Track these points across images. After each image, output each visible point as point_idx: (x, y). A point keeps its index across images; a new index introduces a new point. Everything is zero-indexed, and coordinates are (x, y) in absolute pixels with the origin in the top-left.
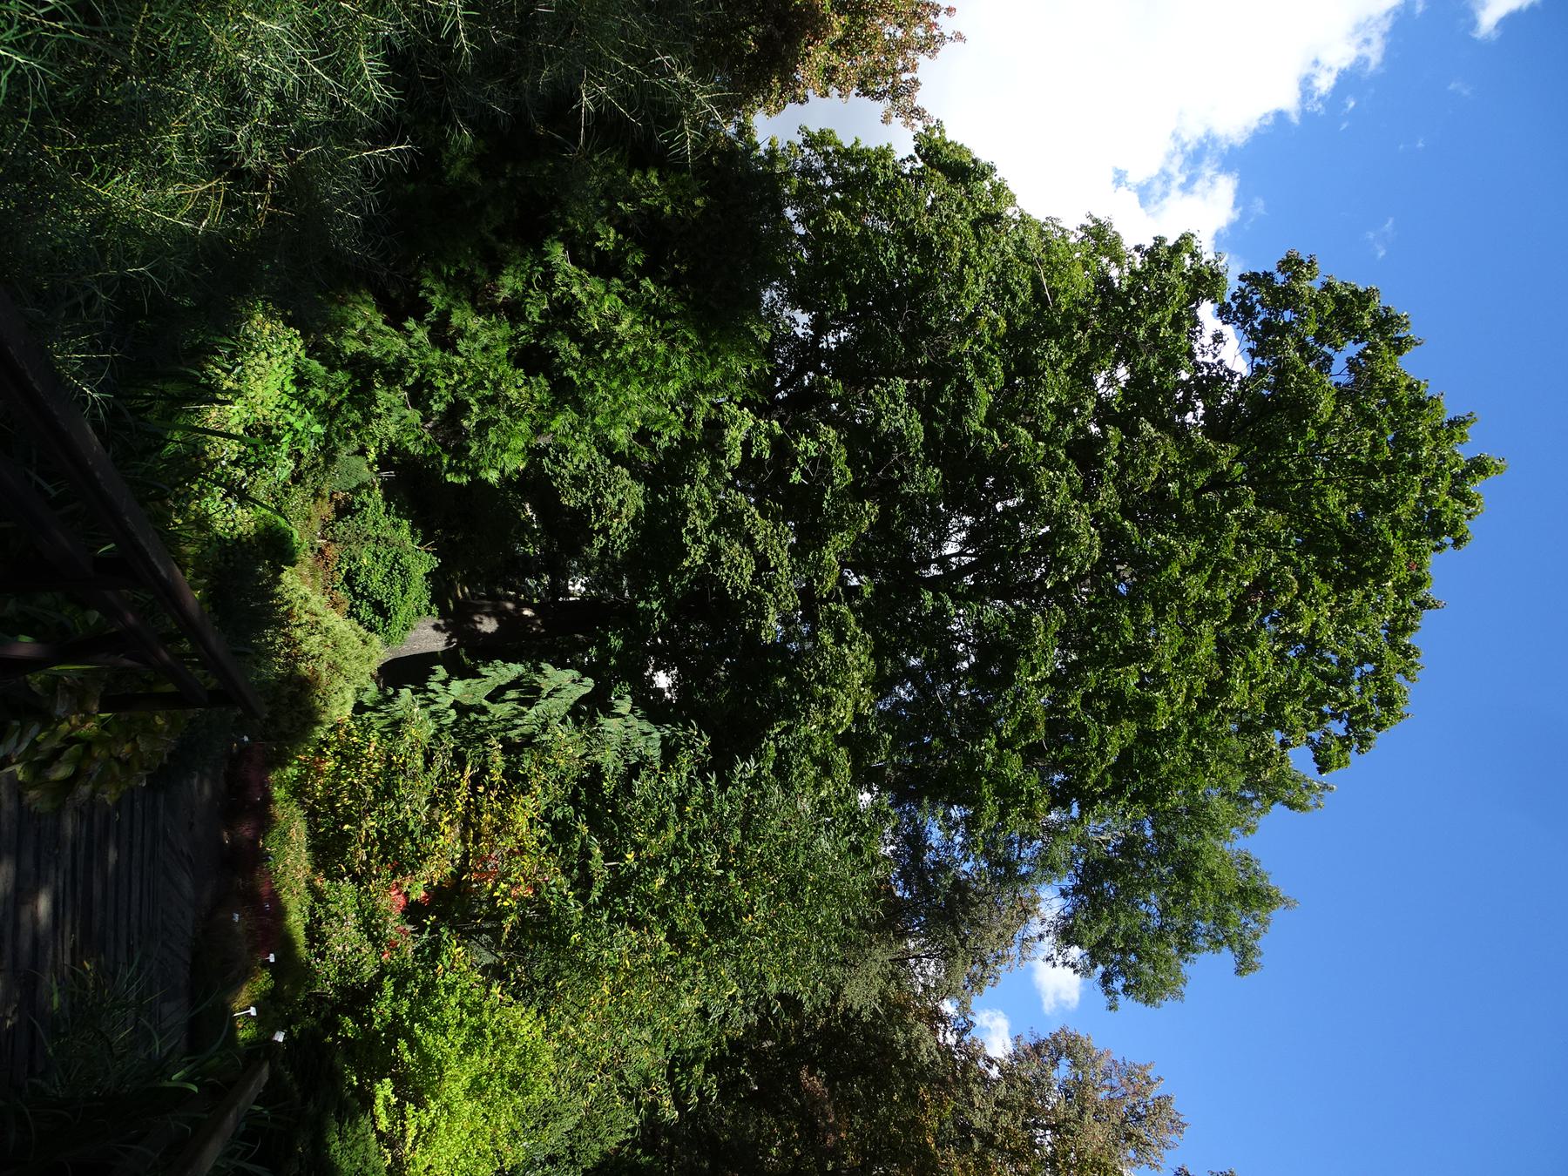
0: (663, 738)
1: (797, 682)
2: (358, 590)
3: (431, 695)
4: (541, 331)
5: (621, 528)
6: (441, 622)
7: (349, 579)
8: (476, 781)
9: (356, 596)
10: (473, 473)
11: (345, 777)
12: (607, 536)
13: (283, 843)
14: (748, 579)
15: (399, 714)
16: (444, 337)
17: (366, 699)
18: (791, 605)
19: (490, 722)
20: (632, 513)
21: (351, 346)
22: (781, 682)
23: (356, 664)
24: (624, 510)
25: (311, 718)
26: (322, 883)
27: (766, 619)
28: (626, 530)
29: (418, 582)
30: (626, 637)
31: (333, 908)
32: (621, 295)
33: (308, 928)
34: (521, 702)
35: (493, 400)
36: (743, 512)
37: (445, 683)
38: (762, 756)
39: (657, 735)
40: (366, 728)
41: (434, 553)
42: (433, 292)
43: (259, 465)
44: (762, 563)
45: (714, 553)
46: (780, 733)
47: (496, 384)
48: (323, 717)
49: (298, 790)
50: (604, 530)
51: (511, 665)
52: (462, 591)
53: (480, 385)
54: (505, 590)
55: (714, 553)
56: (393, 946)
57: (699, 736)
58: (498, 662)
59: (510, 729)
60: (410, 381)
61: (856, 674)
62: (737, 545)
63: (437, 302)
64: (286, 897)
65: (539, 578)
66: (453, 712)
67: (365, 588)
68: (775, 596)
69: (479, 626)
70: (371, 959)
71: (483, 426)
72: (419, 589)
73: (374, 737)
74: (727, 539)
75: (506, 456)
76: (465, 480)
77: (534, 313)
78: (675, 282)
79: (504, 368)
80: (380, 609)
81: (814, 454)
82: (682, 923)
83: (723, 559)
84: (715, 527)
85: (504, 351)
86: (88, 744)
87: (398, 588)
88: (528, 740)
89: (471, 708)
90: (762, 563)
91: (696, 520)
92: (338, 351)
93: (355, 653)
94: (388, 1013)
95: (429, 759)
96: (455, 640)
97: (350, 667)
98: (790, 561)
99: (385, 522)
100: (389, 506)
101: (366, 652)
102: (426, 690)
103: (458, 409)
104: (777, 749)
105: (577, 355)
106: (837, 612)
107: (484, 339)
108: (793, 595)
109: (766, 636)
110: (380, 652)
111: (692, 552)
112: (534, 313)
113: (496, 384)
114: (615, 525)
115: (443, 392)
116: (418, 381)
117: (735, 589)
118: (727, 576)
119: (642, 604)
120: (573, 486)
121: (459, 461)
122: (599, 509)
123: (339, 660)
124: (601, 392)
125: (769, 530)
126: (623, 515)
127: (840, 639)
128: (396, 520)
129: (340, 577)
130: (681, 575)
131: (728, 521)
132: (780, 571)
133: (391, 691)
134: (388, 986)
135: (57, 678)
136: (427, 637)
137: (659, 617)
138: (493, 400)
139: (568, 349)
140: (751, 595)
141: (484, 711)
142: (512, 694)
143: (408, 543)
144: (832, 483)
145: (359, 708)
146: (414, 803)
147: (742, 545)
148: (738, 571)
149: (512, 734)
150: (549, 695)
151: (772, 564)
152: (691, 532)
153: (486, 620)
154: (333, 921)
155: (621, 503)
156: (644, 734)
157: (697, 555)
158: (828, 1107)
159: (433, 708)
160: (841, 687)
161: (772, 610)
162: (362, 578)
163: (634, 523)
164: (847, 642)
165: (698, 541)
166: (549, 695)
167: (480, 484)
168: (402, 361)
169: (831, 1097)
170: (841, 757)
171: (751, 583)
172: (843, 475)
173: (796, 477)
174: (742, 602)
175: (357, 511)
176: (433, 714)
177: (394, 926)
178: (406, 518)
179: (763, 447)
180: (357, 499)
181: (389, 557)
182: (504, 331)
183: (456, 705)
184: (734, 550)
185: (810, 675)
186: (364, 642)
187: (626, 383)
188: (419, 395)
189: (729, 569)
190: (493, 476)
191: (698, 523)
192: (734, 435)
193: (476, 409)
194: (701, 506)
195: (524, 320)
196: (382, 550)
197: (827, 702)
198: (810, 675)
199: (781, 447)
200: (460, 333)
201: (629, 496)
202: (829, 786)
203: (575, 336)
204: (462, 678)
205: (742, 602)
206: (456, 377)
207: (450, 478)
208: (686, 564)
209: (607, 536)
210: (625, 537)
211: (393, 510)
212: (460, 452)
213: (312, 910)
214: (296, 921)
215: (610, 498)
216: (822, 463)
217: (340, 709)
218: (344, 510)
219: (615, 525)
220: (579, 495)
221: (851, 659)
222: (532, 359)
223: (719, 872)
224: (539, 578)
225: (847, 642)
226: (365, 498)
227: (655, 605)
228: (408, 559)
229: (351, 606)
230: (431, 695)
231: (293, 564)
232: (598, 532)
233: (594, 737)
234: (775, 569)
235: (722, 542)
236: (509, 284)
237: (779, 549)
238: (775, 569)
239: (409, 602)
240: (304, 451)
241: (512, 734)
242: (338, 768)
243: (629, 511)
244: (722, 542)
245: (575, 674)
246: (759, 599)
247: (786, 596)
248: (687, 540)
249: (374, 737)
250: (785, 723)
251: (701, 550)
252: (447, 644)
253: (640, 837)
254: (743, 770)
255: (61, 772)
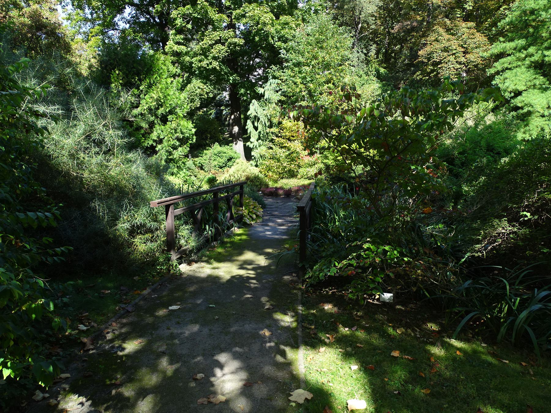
0: (272, 79)
1: (258, 33)
2: (224, 165)
3: (254, 147)
4: (157, 117)
5: (207, 88)
6: (234, 143)
7: (221, 168)
8: (277, 136)
9: (225, 166)
10: (193, 135)
11: (274, 170)
12: (209, 93)
13: (287, 185)
14: (223, 47)
15: (259, 156)
16: (160, 141)
17: (254, 164)
18: (232, 33)
19: (263, 131)
20: (202, 84)
21: (163, 163)
22: (257, 39)
23: (243, 166)
24: (201, 87)
25: (257, 178)
26: (299, 176)
27: (236, 42)
28: (207, 86)
29: (222, 149)
30: (242, 87)
31: (305, 173)
32: (145, 95)
33: (309, 179)
34: (258, 121)
35: (176, 130)
36: (201, 47)
37: (251, 142)
38: (280, 47)
39: (271, 80)
40: (261, 164)
41: (214, 144)
42: (148, 143)
43: (193, 183)
44: (218, 42)
45: (215, 58)
46: (273, 40)
47: (172, 129)
48: (257, 174)
49: (276, 181)
50: (207, 93)
51: (247, 124)
52: (227, 135)
53: (172, 133)
54: (152, 315)
55: (215, 58)
56: (316, 160)
57: (271, 69)
58: (246, 128)
59: (266, 125)
60: (172, 150)
61: (256, 11)
62: (212, 50)
63: (151, 142)
64: (300, 184)
65: (222, 110)
66: (259, 141)
67: (224, 163)
68: (229, 38)
69: (236, 132)
70: (319, 165)
71: (182, 133)
72: (225, 149)
73: (264, 162)
74: (210, 53)
75: (189, 127)
76: (195, 137)
77: (152, 118)
78: (140, 80)
79: (167, 126)
80: (230, 159)
81: (182, 19)
82: (324, 80)
83: (217, 55)
84: (206, 57)
85: (163, 127)
86: (249, 212)
87: (224, 155)
88: (269, 120)
89: (259, 136)
90: (218, 42)
91: (204, 64)
92: (164, 166)
93: (240, 165)
94: (332, 161)
95: (271, 148)
96: (240, 139)
97: (244, 167)
98: (218, 31)
99: (205, 157)
100: (200, 156)
101: (240, 163)
102: (253, 148)
103: (178, 139)
104: (279, 41)
105: (163, 108)
106: (235, 16)
107: (160, 132)
108: (229, 32)
109: (242, 42)
110: (242, 159)
111: (214, 66)
112: (152, 118)
113: (172, 129)
114: (206, 90)
115: (174, 142)
116: (172, 148)
117: (227, 52)
118: (222, 54)
119: (231, 81)
120: (194, 102)
121: (190, 138)
122: (201, 95)
123: (242, 170)
124: (171, 102)
125: (208, 38)
126: (203, 87)
127: (244, 16)
128: (204, 154)
129: (220, 170)
130: (222, 69)
131: (205, 52)
132: (221, 35)
133: (253, 158)
134: (325, 161)
135: (235, 213)
136: (238, 147)
137: (235, 77)
138: (176, 130)
139: (161, 111)
140: (229, 47)
141: (260, 132)
142: (256, 124)
143: (210, 151)
144: (191, 14)
145: (256, 166)
146: (282, 153)
147: (212, 48)
148: (220, 50)
149: (267, 125)
150: (257, 113)
151: (219, 38)
152: (208, 65)
153: (234, 130)
154: (308, 173)
155: (199, 88)
156: (271, 84)
157: (215, 64)
158: (405, 23)
159: (257, 146)
160: (260, 18)
161: (233, 40)
162: (221, 164)
163: (205, 84)
164: (245, 14)
165: (211, 63)
166: (257, 113)
167: (196, 134)
168: (167, 151)
169: (402, 22)
170: (283, 18)
171: (225, 46)
172: (188, 9)
173: (189, 26)
174: (231, 50)
175: (202, 164)
176: (259, 146)
177: (312, 159)
178: (203, 151)
179: (180, 37)
180: (198, 165)
181: (215, 156)
182: (157, 126)
183: (257, 141)
184: (214, 51)
185: (255, 29)
186: (238, 164)
187: (168, 95)
188: (175, 148)
189: (220, 53)
190: (194, 130)
191: (205, 63)
192: (176, 48)
193: (178, 134)
194: (200, 61)
195: (153, 121)
196: (213, 158)
197: (265, 24)
198: (255, 29)
199: (180, 31)
200: (158, 137)
201: (196, 84)
202: (292, 24)
203: (158, 109)
204: (250, 138)
205: (231, 50)
206: (170, 139)
207: (194, 141)
208: (218, 68)
209: (209, 93)
210: (210, 87)
211: (201, 155)
212: (188, 138)
213: (305, 178)
214: (307, 182)
215: (197, 91)
216: (184, 16)
217: (256, 171)
218: (201, 168)
219: (206, 90)
220: (196, 101)
221: (250, 14)
222: (164, 120)
223: (311, 67)
224: (222, 110)
225: (245, 14)
226: (198, 162)
227: (231, 78)
228: (216, 152)
229: (229, 167)
230: (254, 147)
231: (216, 177)
232: (208, 95)
233: (269, 101)
234: (220, 37)
235: (211, 55)
236: (144, 125)
237: (214, 35)
238: (220, 37)
239: (228, 151)
240: (189, 174)
241: (267, 125)
242: (272, 172)
243: (201, 85)
244: (211, 55)
245: (251, 104)
246: (230, 44)
247: (229, 34)
248: (210, 67)
249: (264, 162)
250: (270, 38)
251: (214, 63)
252: (241, 141)
253: (298, 90)
254: (283, 54)
255: (254, 216)
